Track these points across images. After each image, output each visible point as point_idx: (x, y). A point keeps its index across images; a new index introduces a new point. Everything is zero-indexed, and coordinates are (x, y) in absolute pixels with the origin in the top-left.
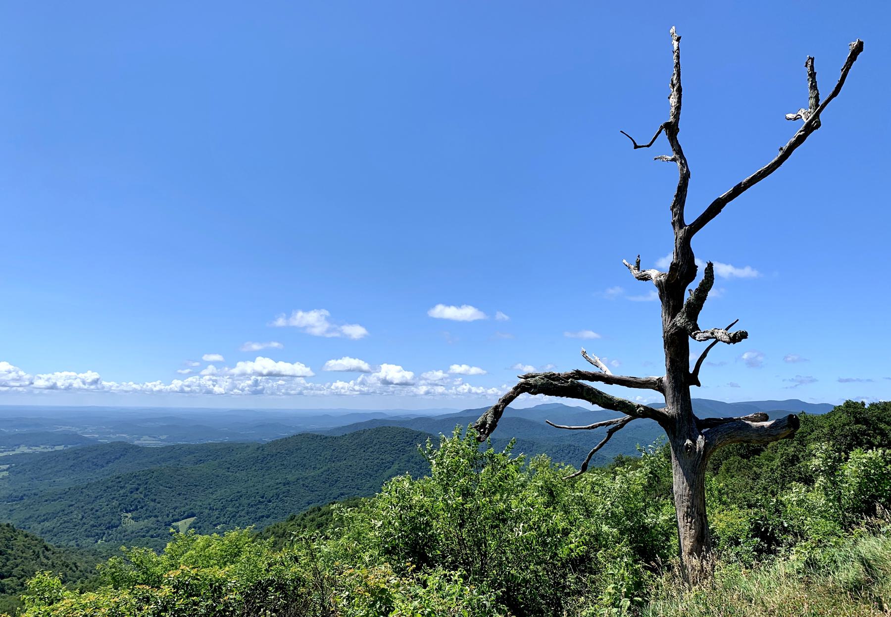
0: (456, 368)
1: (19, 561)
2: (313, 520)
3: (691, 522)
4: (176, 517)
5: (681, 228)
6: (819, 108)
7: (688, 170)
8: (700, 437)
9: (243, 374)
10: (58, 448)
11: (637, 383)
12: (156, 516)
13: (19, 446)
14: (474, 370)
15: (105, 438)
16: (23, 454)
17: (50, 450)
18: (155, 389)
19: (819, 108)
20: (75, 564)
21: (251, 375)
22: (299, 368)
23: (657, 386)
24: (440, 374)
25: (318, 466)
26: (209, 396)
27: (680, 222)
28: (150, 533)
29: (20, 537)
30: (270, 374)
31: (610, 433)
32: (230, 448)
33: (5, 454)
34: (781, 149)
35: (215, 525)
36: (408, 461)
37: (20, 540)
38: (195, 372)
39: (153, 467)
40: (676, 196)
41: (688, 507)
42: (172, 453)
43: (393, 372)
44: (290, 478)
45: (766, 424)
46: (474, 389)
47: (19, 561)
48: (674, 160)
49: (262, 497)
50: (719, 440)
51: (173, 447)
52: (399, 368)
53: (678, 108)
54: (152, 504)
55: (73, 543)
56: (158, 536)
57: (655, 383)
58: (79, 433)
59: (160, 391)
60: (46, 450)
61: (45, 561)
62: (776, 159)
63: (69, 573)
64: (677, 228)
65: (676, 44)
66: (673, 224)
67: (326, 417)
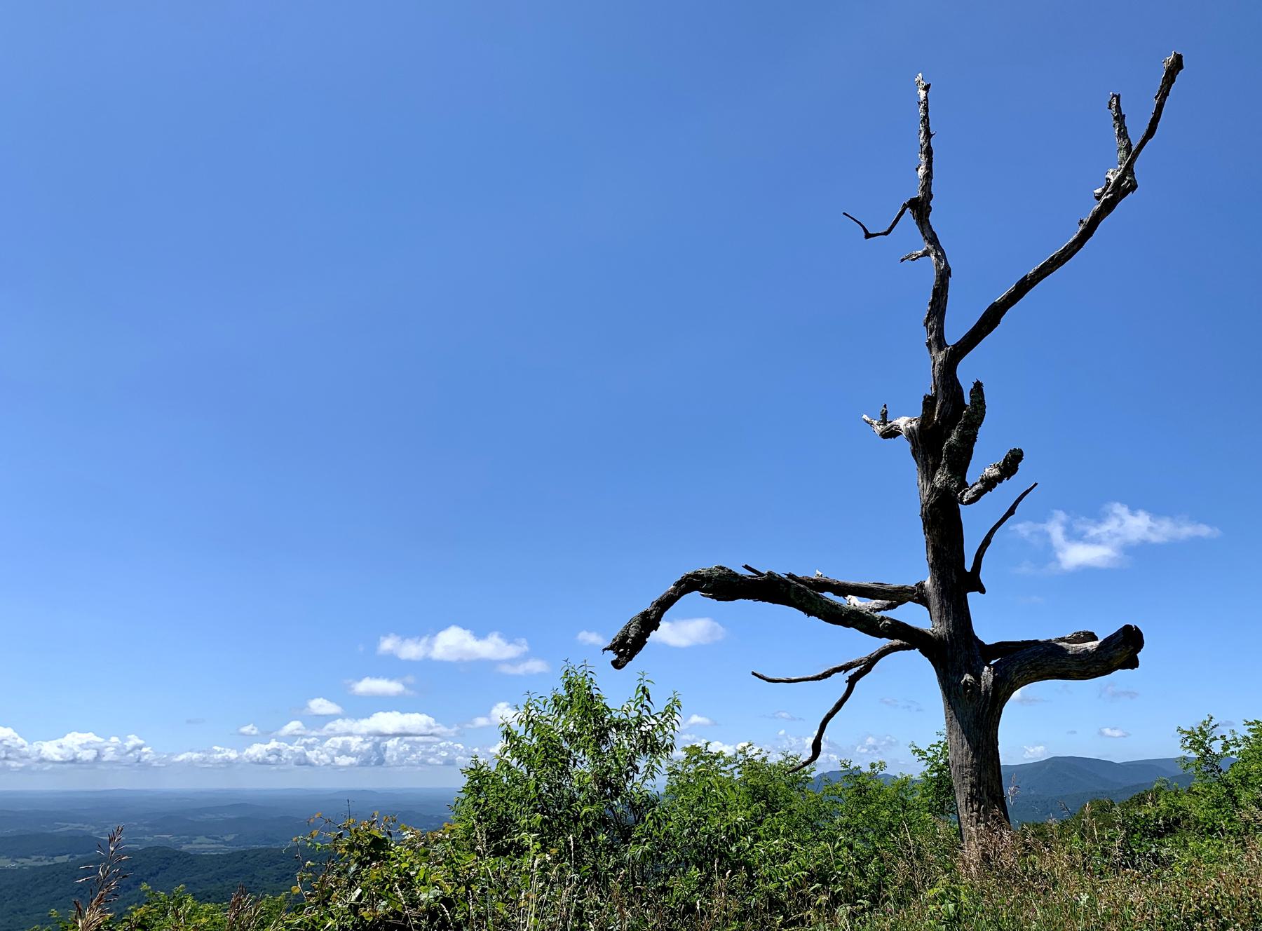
3: (978, 811)
5: (940, 349)
6: (1133, 154)
7: (947, 265)
8: (986, 668)
10: (59, 860)
11: (884, 591)
15: (136, 841)
17: (47, 863)
19: (1133, 154)
23: (918, 595)
26: (306, 769)
27: (940, 342)
31: (852, 681)
34: (1081, 222)
40: (932, 304)
41: (972, 786)
45: (1091, 645)
48: (926, 254)
50: (1018, 672)
51: (244, 855)
53: (928, 176)
57: (912, 591)
58: (95, 833)
60: (39, 864)
62: (1075, 236)
64: (934, 350)
65: (922, 94)
66: (929, 345)
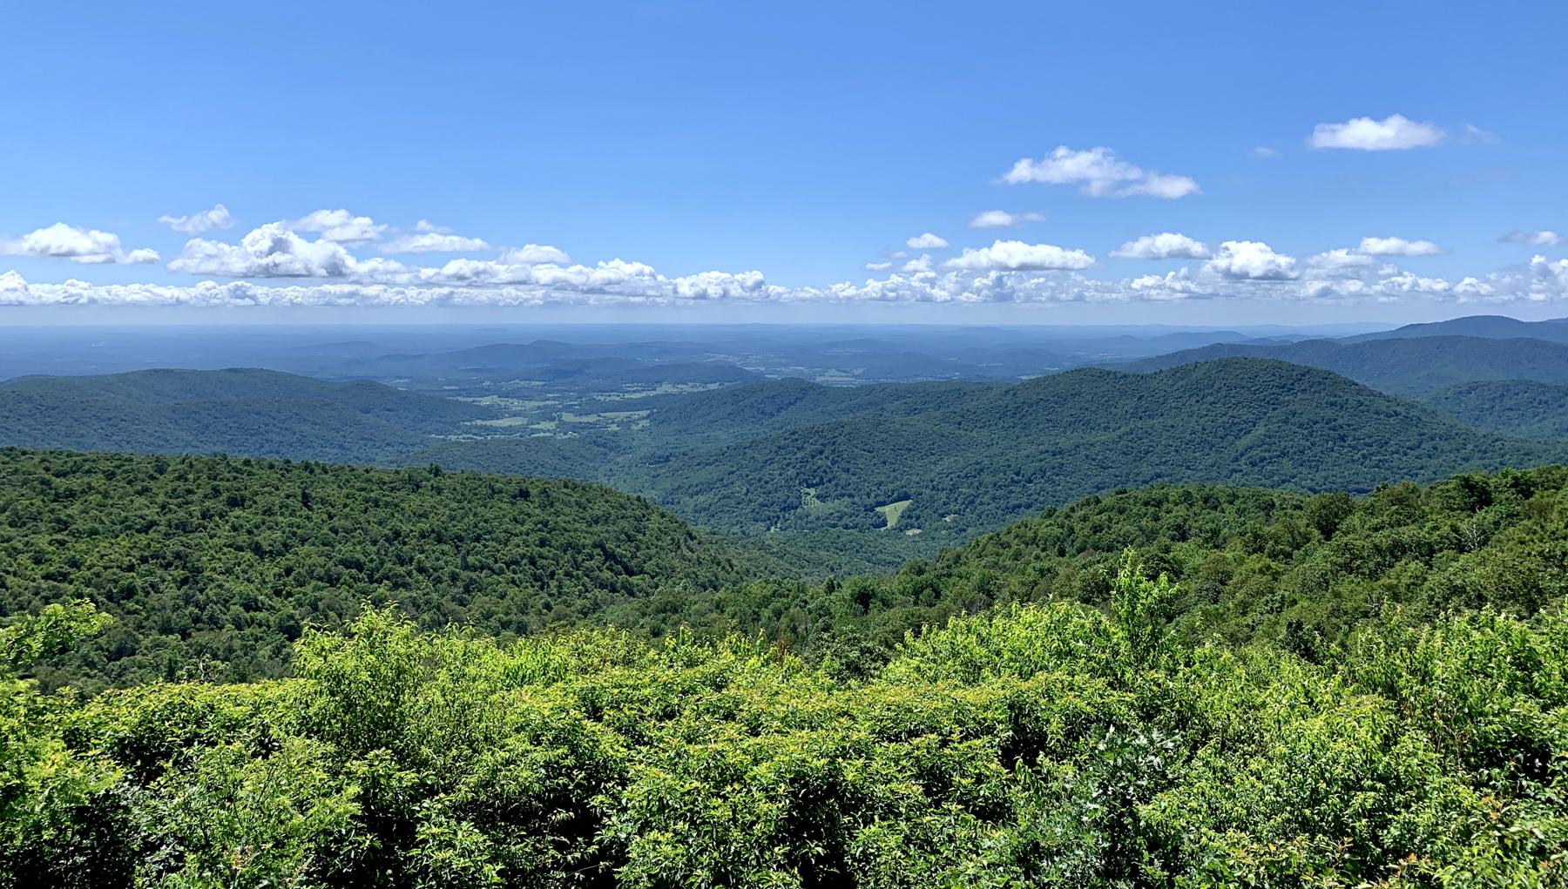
0: (1374, 245)
1: (653, 551)
2: (1085, 519)
4: (881, 499)
9: (976, 271)
10: (712, 387)
12: (851, 496)
13: (660, 382)
14: (1420, 247)
16: (666, 395)
18: (841, 295)
20: (729, 561)
21: (988, 270)
22: (1077, 258)
24: (1341, 256)
25: (1112, 425)
26: (926, 305)
28: (845, 520)
29: (655, 517)
30: (1023, 267)
32: (959, 392)
33: (644, 394)
35: (943, 516)
36: (1286, 422)
37: (654, 523)
38: (896, 269)
39: (845, 419)
42: (872, 397)
43: (1250, 256)
44: (1064, 443)
46: (1424, 283)
47: (653, 551)
49: (1018, 474)
51: (871, 389)
52: (1261, 245)
54: (844, 476)
55: (736, 529)
56: (855, 527)
59: (849, 299)
61: (689, 554)
63: (721, 574)
67: (1127, 338)
